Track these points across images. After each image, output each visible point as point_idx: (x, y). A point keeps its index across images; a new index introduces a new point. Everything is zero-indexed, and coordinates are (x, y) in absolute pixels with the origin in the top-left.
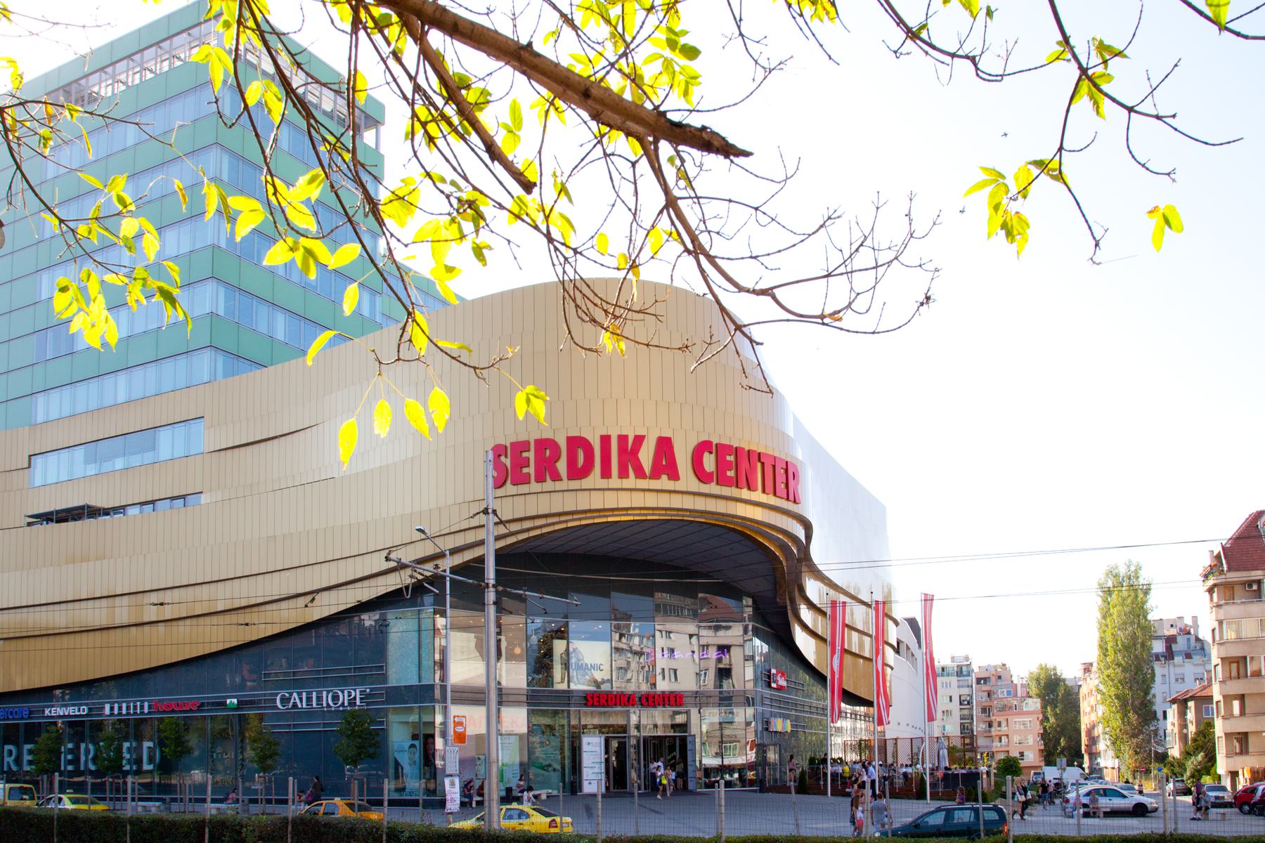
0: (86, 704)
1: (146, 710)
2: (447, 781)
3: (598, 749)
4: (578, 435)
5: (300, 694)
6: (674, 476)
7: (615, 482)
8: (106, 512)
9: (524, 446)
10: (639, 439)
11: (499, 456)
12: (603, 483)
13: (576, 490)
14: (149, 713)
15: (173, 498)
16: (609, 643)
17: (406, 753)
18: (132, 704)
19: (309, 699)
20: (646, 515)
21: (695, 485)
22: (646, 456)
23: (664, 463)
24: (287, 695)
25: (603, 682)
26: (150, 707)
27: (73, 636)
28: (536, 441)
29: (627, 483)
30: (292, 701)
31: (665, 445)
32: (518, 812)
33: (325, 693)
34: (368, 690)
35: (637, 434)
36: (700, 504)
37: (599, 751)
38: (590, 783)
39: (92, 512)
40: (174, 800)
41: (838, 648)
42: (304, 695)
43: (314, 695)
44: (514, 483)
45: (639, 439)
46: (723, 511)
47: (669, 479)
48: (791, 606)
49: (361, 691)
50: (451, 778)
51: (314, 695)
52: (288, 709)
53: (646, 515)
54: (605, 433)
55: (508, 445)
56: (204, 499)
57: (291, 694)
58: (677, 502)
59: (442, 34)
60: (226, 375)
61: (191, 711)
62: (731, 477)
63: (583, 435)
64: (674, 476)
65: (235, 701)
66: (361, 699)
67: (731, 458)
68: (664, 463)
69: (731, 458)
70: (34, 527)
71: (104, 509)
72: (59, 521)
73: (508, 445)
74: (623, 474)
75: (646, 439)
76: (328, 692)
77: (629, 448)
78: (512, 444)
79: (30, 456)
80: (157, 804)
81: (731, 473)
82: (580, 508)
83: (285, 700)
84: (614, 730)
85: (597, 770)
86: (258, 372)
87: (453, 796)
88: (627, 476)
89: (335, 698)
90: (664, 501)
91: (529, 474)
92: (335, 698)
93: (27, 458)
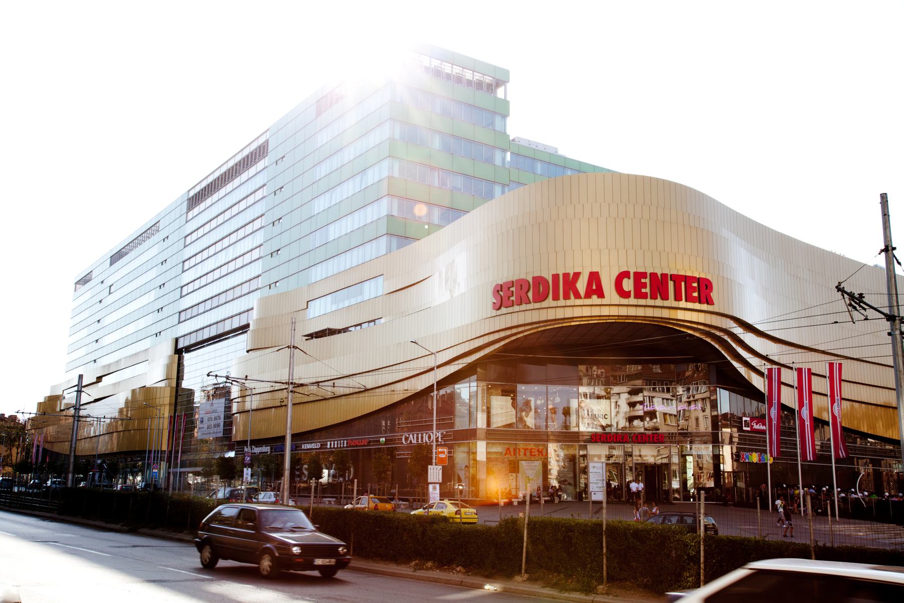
1: (345, 445)
2: (431, 487)
3: (600, 471)
4: (539, 275)
5: (413, 435)
6: (601, 295)
7: (562, 302)
8: (339, 331)
9: (644, 275)
10: (577, 275)
11: (498, 291)
12: (554, 303)
13: (539, 309)
14: (347, 447)
15: (369, 322)
16: (577, 400)
17: (463, 471)
18: (339, 442)
19: (417, 438)
21: (617, 299)
23: (594, 287)
24: (407, 436)
25: (608, 426)
26: (347, 443)
27: (318, 402)
28: (564, 274)
29: (569, 302)
30: (410, 439)
31: (594, 277)
33: (424, 434)
34: (445, 432)
35: (575, 271)
36: (623, 311)
37: (601, 472)
38: (595, 494)
39: (330, 332)
40: (414, 500)
41: (775, 401)
42: (415, 435)
43: (420, 435)
44: (636, 297)
45: (577, 275)
49: (442, 433)
50: (434, 485)
51: (420, 435)
52: (407, 444)
54: (555, 273)
55: (531, 281)
56: (382, 321)
57: (409, 435)
58: (605, 311)
60: (398, 248)
61: (364, 445)
63: (707, 278)
65: (384, 439)
66: (441, 437)
67: (695, 285)
69: (695, 285)
70: (308, 341)
71: (339, 330)
72: (316, 337)
73: (514, 280)
74: (566, 297)
75: (582, 274)
76: (426, 433)
77: (570, 281)
78: (516, 280)
79: (308, 302)
80: (334, 499)
82: (557, 318)
83: (406, 439)
84: (307, 454)
85: (600, 485)
86: (418, 242)
87: (434, 495)
89: (429, 437)
90: (596, 311)
91: (646, 283)
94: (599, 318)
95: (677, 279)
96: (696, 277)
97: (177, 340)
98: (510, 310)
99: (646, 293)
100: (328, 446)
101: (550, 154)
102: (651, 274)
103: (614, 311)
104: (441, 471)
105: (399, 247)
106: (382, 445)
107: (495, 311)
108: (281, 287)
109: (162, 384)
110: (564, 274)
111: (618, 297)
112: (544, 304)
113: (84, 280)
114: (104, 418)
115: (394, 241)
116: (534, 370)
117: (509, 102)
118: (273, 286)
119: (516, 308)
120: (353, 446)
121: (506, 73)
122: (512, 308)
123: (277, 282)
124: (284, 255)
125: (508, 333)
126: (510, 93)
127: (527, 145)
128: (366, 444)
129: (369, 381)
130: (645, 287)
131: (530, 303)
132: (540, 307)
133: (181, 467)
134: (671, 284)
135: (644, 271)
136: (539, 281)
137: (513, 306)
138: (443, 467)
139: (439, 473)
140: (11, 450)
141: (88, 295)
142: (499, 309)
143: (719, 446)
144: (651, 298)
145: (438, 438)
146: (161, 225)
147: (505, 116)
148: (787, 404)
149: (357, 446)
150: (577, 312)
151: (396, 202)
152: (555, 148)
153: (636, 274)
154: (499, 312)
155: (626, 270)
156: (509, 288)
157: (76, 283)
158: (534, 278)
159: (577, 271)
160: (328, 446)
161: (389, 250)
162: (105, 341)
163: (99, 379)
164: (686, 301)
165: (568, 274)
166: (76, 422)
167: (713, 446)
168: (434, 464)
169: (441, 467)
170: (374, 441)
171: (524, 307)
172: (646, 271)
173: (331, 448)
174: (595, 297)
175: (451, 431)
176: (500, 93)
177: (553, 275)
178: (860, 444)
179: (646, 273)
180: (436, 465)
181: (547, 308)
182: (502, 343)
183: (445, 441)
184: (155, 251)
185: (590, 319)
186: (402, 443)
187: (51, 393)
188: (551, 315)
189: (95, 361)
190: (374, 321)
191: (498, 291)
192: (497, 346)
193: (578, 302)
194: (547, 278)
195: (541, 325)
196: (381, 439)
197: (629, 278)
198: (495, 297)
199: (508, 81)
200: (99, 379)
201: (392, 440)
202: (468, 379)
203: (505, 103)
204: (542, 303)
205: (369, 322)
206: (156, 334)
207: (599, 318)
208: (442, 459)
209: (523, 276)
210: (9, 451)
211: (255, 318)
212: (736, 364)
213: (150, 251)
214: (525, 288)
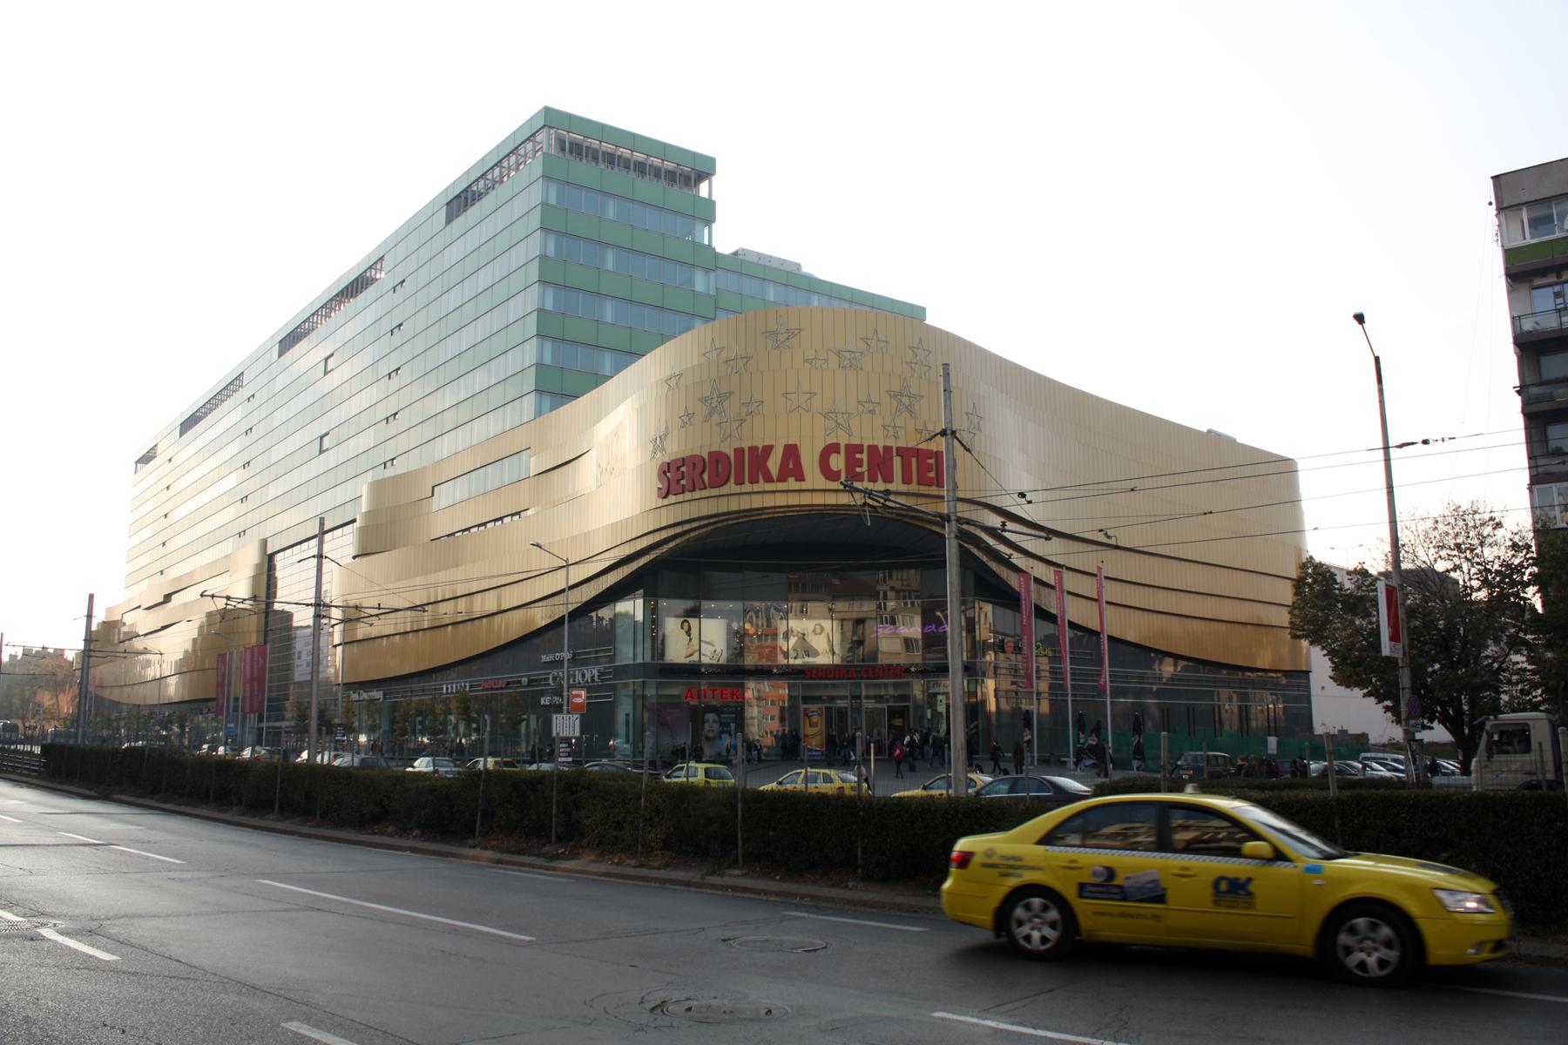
0: (470, 682)
4: (718, 449)
6: (800, 477)
7: (747, 487)
9: (859, 449)
10: (768, 449)
12: (737, 489)
15: (512, 515)
20: (738, 518)
21: (821, 482)
22: (774, 464)
23: (791, 466)
28: (749, 448)
29: (757, 487)
31: (791, 452)
32: (704, 759)
33: (577, 672)
45: (768, 449)
46: (735, 508)
47: (797, 480)
48: (978, 547)
53: (738, 518)
55: (706, 456)
56: (529, 513)
58: (806, 499)
59: (1390, 550)
61: (502, 688)
62: (932, 478)
64: (888, 479)
65: (526, 679)
67: (932, 461)
68: (791, 466)
69: (932, 461)
74: (754, 481)
81: (932, 474)
82: (730, 510)
88: (757, 482)
89: (583, 676)
90: (794, 500)
91: (861, 460)
92: (583, 676)
93: (699, 477)
94: (798, 509)
95: (904, 453)
96: (932, 451)
97: (264, 543)
98: (680, 498)
99: (862, 473)
100: (444, 691)
101: (788, 272)
102: (869, 447)
103: (818, 499)
104: (578, 722)
105: (553, 408)
106: (524, 687)
107: (661, 500)
108: (400, 467)
109: (246, 605)
110: (749, 448)
111: (823, 478)
112: (725, 490)
113: (146, 459)
114: (125, 652)
115: (547, 401)
116: (720, 577)
117: (714, 202)
118: (389, 464)
119: (688, 496)
120: (487, 690)
121: (711, 161)
122: (682, 496)
123: (394, 458)
124: (403, 421)
125: (678, 530)
126: (717, 189)
127: (756, 260)
128: (504, 686)
129: (488, 603)
130: (861, 466)
131: (705, 488)
132: (682, 500)
133: (268, 721)
134: (897, 462)
135: (859, 442)
136: (717, 457)
137: (683, 492)
138: (582, 716)
139: (574, 724)
140: (57, 698)
141: (151, 479)
142: (665, 497)
143: (977, 680)
144: (869, 481)
145: (594, 676)
146: (246, 379)
147: (709, 220)
148: (1076, 622)
149: (492, 689)
150: (769, 501)
151: (548, 347)
152: (796, 263)
153: (848, 446)
154: (666, 502)
155: (835, 441)
156: (678, 468)
157: (137, 462)
158: (710, 453)
159: (767, 443)
160: (444, 691)
161: (539, 413)
162: (175, 544)
163: (167, 598)
164: (919, 484)
165: (757, 448)
166: (86, 658)
167: (968, 680)
168: (565, 711)
169: (578, 716)
170: (514, 682)
171: (697, 494)
172: (875, 444)
173: (447, 693)
174: (791, 480)
175: (610, 668)
176: (703, 190)
177: (735, 449)
178: (860, 683)
179: (862, 446)
180: (568, 713)
181: (728, 495)
182: (671, 545)
183: (603, 680)
184: (237, 415)
185: (786, 509)
186: (549, 684)
187: (106, 618)
188: (734, 505)
189: (162, 572)
190: (518, 513)
191: (664, 472)
192: (665, 548)
193: (770, 487)
194: (728, 454)
195: (732, 516)
196: (523, 679)
197: (839, 453)
198: (660, 480)
199: (713, 173)
200: (167, 598)
201: (536, 680)
202: (632, 596)
203: (710, 205)
204: (721, 488)
205: (512, 515)
206: (240, 534)
207: (798, 509)
208: (578, 704)
209: (697, 452)
210: (54, 700)
211: (363, 510)
212: (993, 566)
213: (229, 416)
214: (699, 467)
